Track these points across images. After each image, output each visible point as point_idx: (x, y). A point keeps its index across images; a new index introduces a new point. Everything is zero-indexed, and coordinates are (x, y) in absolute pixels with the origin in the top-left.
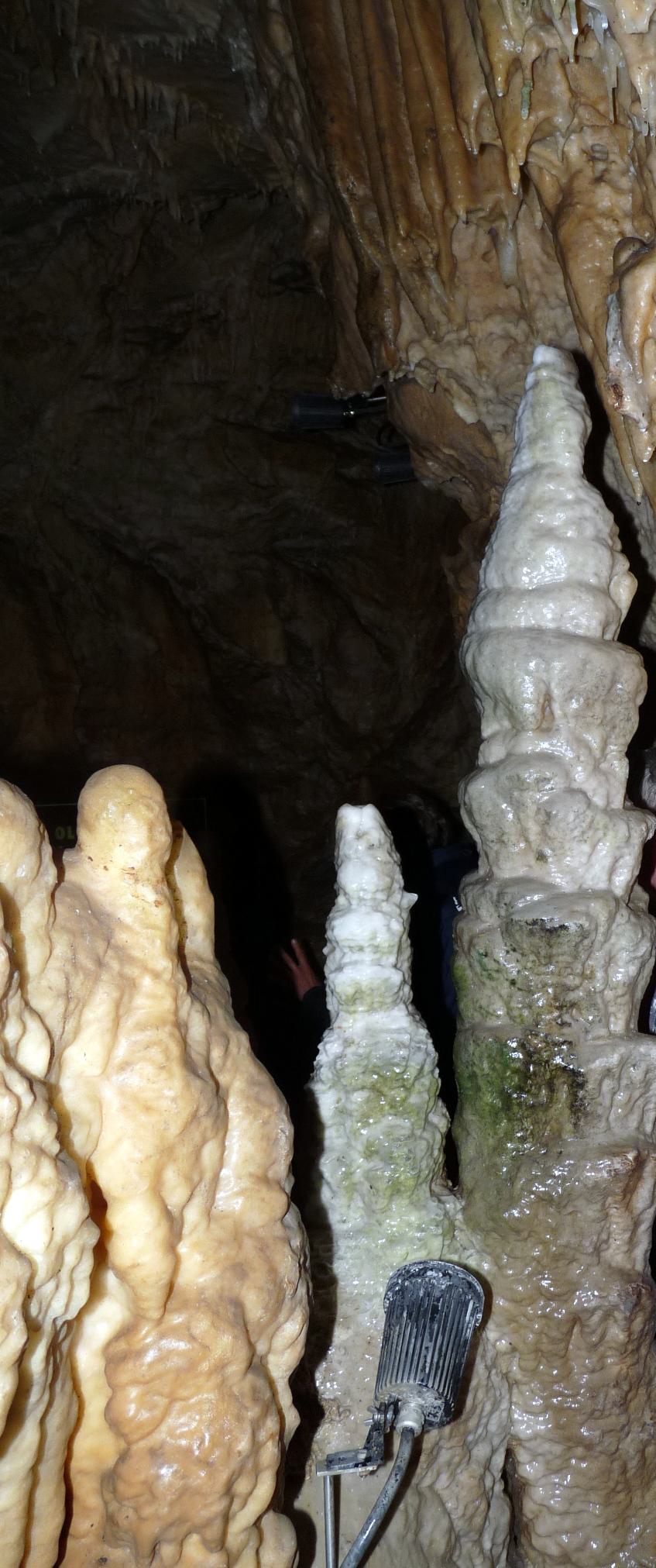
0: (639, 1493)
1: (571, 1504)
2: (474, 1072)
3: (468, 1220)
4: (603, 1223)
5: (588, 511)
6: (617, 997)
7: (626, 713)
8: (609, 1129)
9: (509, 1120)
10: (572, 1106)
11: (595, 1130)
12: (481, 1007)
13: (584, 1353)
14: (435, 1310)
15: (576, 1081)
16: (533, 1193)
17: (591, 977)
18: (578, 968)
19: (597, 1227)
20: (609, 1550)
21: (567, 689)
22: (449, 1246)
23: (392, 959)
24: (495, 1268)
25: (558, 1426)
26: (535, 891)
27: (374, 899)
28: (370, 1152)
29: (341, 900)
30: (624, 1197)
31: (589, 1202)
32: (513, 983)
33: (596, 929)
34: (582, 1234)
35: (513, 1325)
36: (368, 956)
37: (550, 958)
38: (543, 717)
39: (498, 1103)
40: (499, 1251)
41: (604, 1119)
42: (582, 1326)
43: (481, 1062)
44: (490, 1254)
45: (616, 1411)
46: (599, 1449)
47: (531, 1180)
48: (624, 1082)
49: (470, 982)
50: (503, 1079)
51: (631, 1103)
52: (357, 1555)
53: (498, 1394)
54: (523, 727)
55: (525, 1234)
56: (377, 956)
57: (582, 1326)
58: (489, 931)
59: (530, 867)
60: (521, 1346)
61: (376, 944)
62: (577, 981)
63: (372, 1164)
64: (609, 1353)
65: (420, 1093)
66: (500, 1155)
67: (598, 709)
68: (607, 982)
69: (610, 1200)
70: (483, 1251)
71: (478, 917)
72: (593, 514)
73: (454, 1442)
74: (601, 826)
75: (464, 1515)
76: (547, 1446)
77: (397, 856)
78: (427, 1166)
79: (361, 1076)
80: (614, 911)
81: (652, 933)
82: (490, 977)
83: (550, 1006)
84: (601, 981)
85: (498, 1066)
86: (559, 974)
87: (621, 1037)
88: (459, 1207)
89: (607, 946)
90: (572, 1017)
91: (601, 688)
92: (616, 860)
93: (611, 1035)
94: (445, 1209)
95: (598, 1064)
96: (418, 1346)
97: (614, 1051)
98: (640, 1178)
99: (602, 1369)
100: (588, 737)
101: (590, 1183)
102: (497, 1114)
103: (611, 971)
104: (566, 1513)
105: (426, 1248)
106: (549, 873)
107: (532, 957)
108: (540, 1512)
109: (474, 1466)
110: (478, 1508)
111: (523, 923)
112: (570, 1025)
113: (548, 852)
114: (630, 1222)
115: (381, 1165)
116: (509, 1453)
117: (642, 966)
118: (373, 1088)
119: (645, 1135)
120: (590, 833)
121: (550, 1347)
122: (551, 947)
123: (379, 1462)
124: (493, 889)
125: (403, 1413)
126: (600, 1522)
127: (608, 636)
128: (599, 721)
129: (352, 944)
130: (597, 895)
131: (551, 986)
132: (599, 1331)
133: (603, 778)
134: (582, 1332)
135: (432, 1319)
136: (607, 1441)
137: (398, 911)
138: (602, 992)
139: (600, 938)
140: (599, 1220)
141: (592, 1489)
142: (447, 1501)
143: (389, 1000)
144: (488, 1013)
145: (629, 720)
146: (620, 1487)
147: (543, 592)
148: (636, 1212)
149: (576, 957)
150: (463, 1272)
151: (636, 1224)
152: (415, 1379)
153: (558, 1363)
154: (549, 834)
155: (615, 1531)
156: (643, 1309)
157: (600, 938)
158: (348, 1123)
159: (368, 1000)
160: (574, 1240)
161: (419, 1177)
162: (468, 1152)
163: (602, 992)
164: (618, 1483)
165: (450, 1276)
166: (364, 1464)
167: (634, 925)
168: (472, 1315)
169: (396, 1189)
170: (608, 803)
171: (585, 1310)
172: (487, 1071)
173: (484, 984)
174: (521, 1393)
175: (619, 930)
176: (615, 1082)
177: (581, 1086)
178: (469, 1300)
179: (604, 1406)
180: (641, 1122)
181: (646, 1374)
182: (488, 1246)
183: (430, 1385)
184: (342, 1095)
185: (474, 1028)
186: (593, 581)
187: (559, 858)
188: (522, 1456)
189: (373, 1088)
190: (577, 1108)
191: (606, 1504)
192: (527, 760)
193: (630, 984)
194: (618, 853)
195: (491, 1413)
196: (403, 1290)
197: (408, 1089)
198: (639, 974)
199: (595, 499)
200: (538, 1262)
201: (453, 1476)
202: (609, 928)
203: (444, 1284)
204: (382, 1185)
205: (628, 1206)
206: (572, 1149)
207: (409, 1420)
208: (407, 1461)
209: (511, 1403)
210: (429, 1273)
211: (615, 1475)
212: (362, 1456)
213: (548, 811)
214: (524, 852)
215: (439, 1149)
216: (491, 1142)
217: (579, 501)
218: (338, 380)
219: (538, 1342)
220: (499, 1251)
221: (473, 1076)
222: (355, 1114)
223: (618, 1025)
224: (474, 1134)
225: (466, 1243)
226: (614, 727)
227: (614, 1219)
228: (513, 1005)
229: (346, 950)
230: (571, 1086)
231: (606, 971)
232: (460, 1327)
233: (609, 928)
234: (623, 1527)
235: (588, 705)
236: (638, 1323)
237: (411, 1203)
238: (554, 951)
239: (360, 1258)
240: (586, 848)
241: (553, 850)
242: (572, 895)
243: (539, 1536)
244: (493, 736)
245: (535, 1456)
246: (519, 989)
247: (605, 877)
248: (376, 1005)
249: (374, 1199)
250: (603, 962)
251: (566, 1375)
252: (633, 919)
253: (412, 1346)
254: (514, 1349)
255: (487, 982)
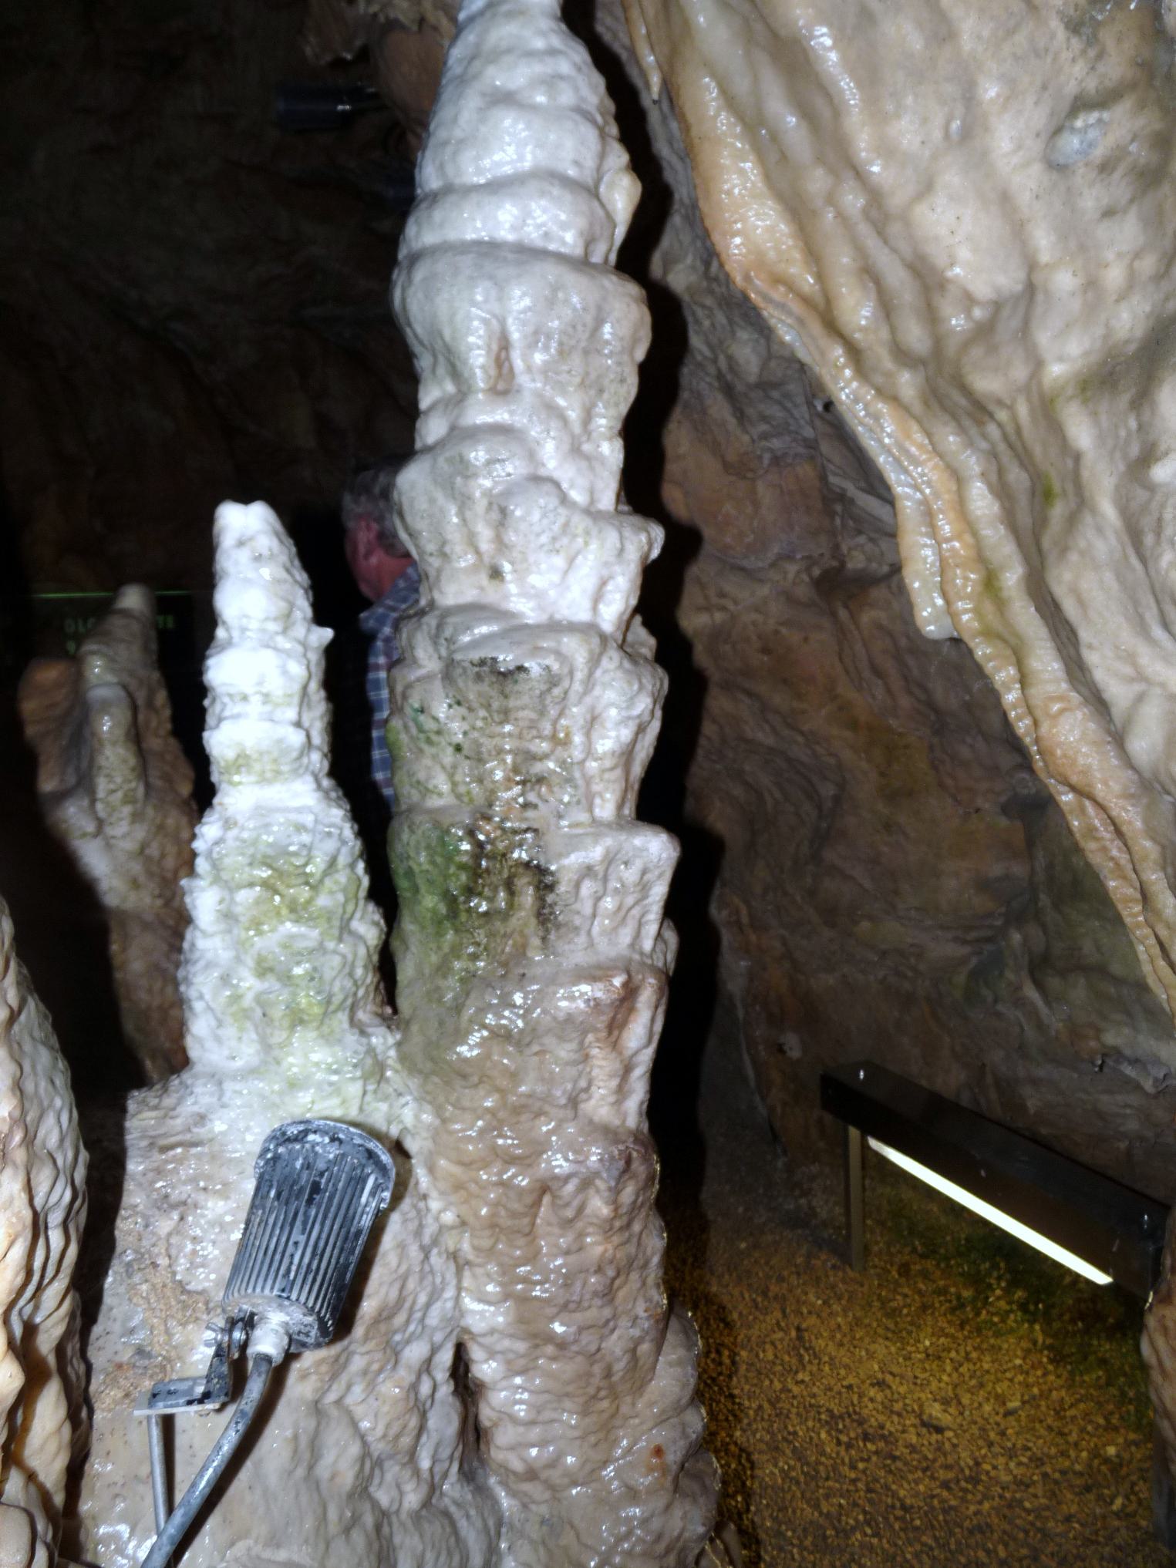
0: (628, 1399)
1: (539, 1412)
2: (410, 867)
3: (403, 1058)
4: (580, 1067)
5: (564, 67)
6: (604, 771)
7: (619, 369)
8: (591, 944)
9: (457, 931)
10: (539, 914)
11: (572, 947)
12: (418, 782)
13: (556, 1230)
14: (316, 1188)
15: (543, 880)
16: (485, 1027)
17: (566, 743)
18: (547, 728)
19: (572, 1071)
20: (588, 1467)
21: (530, 329)
22: (375, 1092)
23: (291, 714)
24: (437, 1122)
25: (521, 1320)
26: (487, 620)
27: (263, 631)
28: (263, 969)
29: (220, 633)
30: (610, 1033)
31: (562, 1039)
32: (458, 748)
33: (571, 673)
34: (550, 1080)
35: (463, 1193)
36: (255, 707)
37: (506, 715)
38: (500, 375)
39: (443, 909)
40: (441, 1099)
41: (583, 933)
42: (554, 1197)
43: (418, 854)
44: (430, 1103)
45: (598, 1302)
46: (575, 1348)
47: (482, 1010)
48: (614, 884)
49: (405, 749)
50: (446, 877)
51: (622, 913)
52: (172, 1537)
53: (438, 1280)
54: (469, 388)
55: (475, 1079)
56: (268, 708)
57: (554, 1197)
58: (429, 678)
59: (482, 589)
60: (471, 1220)
61: (264, 690)
62: (545, 746)
63: (266, 985)
64: (590, 1230)
65: (331, 893)
66: (445, 977)
67: (576, 361)
68: (589, 751)
69: (590, 1037)
70: (424, 1099)
71: (415, 661)
72: (573, 73)
73: (371, 1345)
74: (580, 530)
75: (384, 1436)
76: (506, 1343)
77: (302, 577)
78: (342, 988)
79: (247, 869)
80: (597, 650)
81: (654, 685)
82: (429, 742)
83: (509, 782)
84: (580, 748)
85: (439, 860)
86: (520, 737)
87: (609, 825)
88: (391, 1041)
89: (588, 700)
90: (539, 796)
91: (580, 328)
92: (603, 583)
93: (595, 822)
94: (369, 1044)
95: (574, 860)
96: (284, 1239)
97: (596, 843)
98: (632, 1010)
99: (580, 1249)
100: (561, 402)
101: (561, 1016)
102: (440, 923)
103: (594, 735)
104: (532, 1423)
105: (339, 1094)
106: (507, 597)
107: (482, 713)
108: (500, 1419)
109: (402, 1372)
110: (405, 1427)
111: (466, 664)
112: (535, 807)
113: (507, 567)
114: (618, 1066)
115: (277, 986)
116: (460, 1351)
117: (641, 729)
118: (265, 884)
119: (642, 954)
120: (565, 541)
121: (509, 1223)
122: (506, 697)
123: (223, 1399)
124: (431, 621)
125: (258, 1333)
126: (576, 1433)
127: (597, 258)
128: (578, 380)
129: (232, 691)
130: (572, 628)
131: (510, 752)
132: (576, 1203)
133: (584, 464)
134: (553, 1204)
135: (310, 1201)
136: (585, 1338)
137: (300, 649)
138: (582, 762)
139: (577, 687)
140: (575, 1063)
141: (567, 1395)
142: (361, 1420)
143: (285, 768)
144: (427, 790)
145: (622, 381)
146: (603, 1393)
147: (498, 187)
148: (628, 1053)
149: (542, 713)
150: (360, 1136)
151: (628, 1069)
152: (272, 1288)
153: (521, 1241)
154: (506, 540)
155: (596, 1445)
156: (634, 1176)
157: (577, 687)
158: (236, 931)
159: (257, 767)
160: (540, 1089)
161: (329, 1002)
162: (406, 971)
163: (582, 762)
164: (599, 1389)
165: (341, 1141)
166: (201, 1401)
167: (627, 672)
168: (373, 1194)
169: (297, 1019)
170: (592, 501)
171: (556, 1178)
172: (426, 867)
173: (421, 751)
174: (474, 1276)
175: (607, 678)
176: (600, 883)
177: (550, 888)
178: (369, 1175)
179: (582, 1295)
180: (637, 935)
181: (640, 1256)
182: (427, 1093)
183: (294, 1297)
184: (226, 894)
185: (410, 810)
186: (572, 172)
187: (521, 575)
188: (476, 1353)
189: (265, 884)
190: (544, 916)
191: (584, 1412)
192: (474, 434)
193: (623, 754)
194: (605, 573)
195: (428, 1305)
196: (276, 1158)
197: (315, 888)
198: (634, 742)
199: (579, 54)
200: (494, 1115)
201: (371, 1387)
202: (591, 674)
203: (333, 1152)
204: (278, 1012)
205: (615, 1045)
206: (539, 971)
207: (267, 1343)
208: (255, 1404)
209: (459, 1288)
210: (311, 1137)
211: (596, 1381)
212: (200, 1390)
213: (503, 504)
214: (474, 569)
215: (365, 967)
216: (434, 958)
217: (552, 52)
218: (312, 39)
219: (493, 1215)
220: (441, 1099)
221: (410, 873)
222: (242, 919)
223: (606, 808)
224: (413, 949)
225: (401, 1089)
226: (601, 391)
227: (596, 1062)
228: (458, 778)
229: (226, 700)
230: (537, 888)
231: (588, 734)
232: (351, 1212)
233: (591, 674)
234: (606, 1439)
235: (563, 353)
236: (628, 1194)
237: (322, 1036)
238: (512, 703)
239: (251, 1106)
240: (559, 561)
241: (512, 563)
242: (538, 626)
243: (498, 1448)
244: (432, 407)
245: (492, 1354)
246: (467, 758)
247: (587, 604)
248: (269, 775)
249: (268, 1031)
250: (581, 722)
251: (532, 1257)
252: (627, 664)
253: (275, 1240)
254: (463, 1224)
255: (425, 747)
